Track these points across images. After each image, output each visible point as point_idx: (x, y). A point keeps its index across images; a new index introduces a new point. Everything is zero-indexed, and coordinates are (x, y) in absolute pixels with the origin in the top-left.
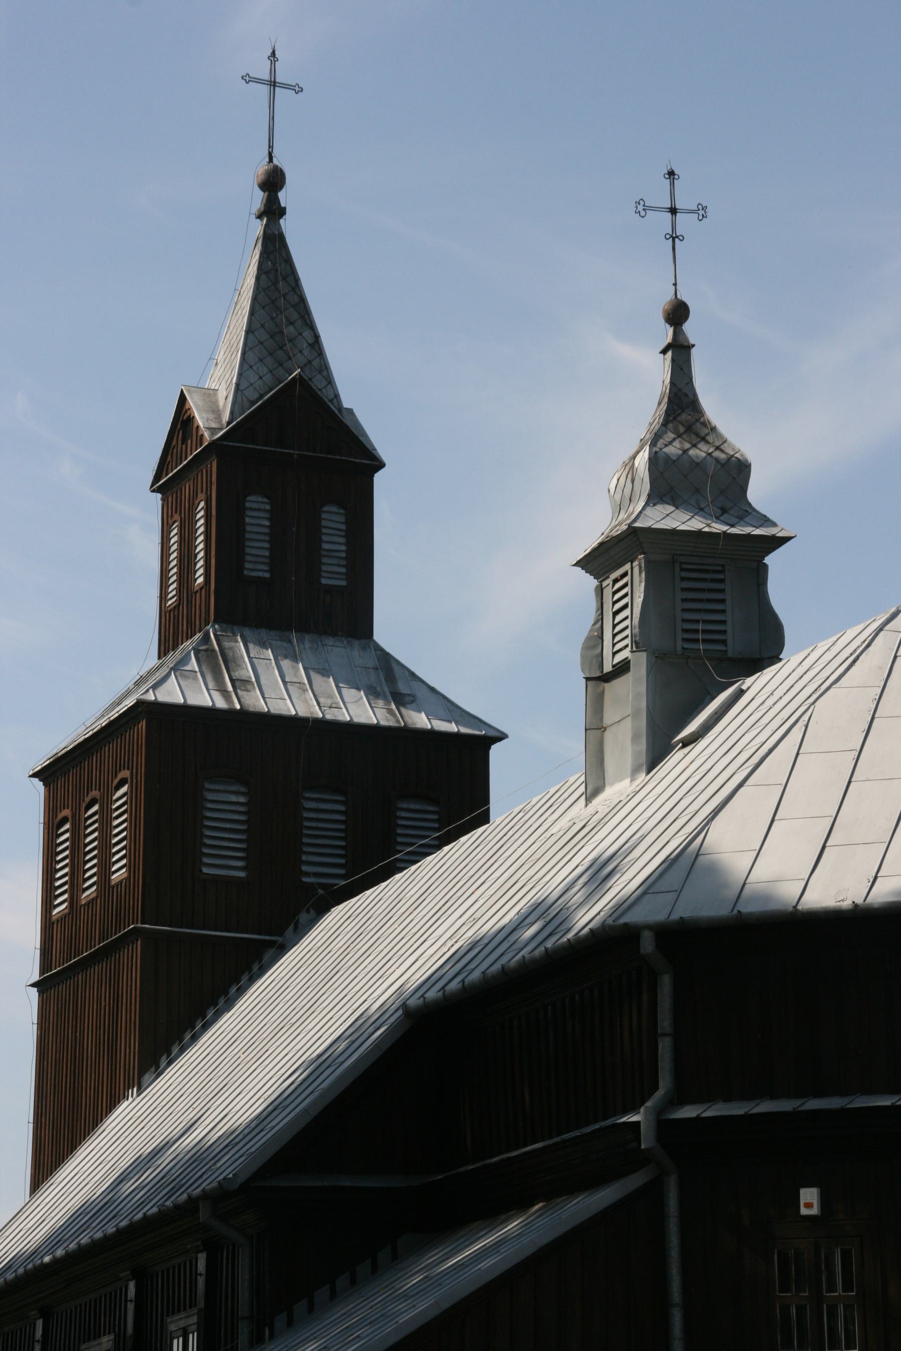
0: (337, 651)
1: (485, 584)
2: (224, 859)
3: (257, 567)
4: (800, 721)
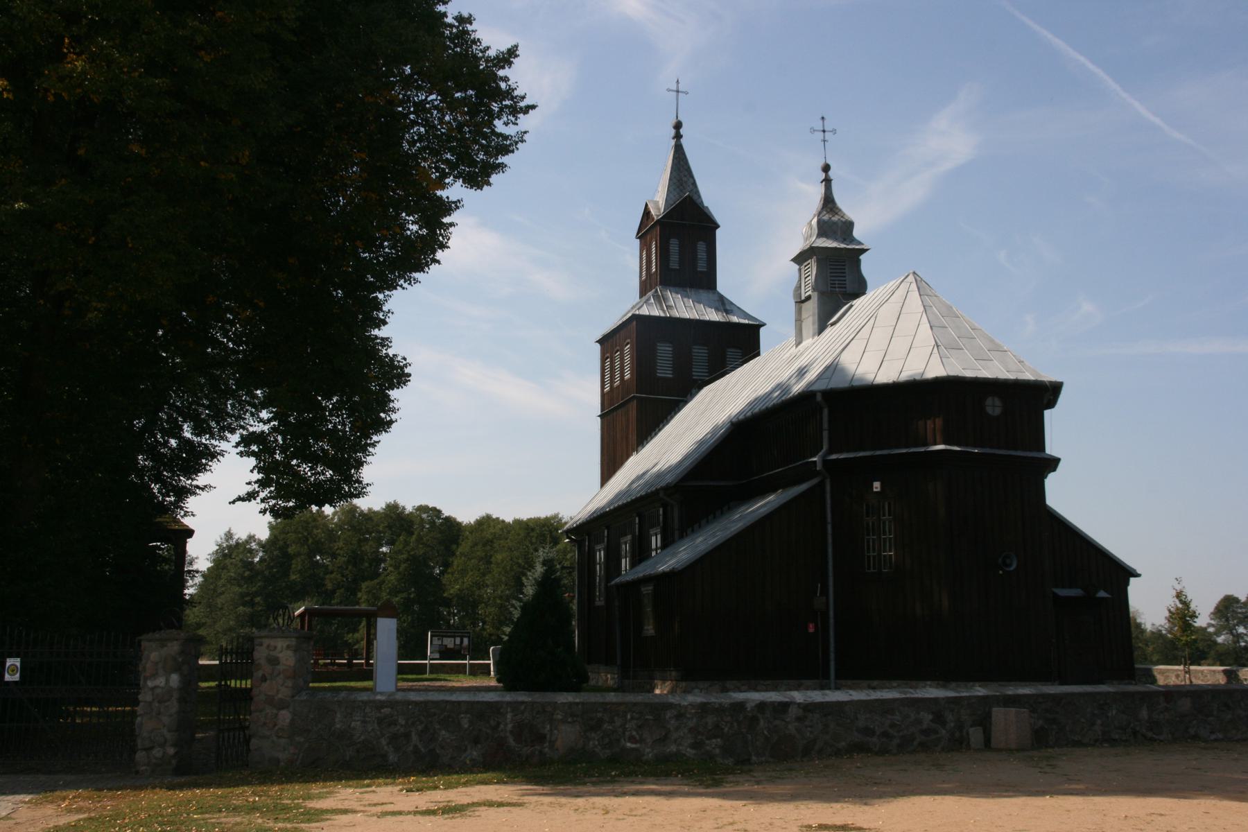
0: (704, 294)
1: (758, 269)
2: (664, 370)
3: (674, 265)
4: (874, 316)
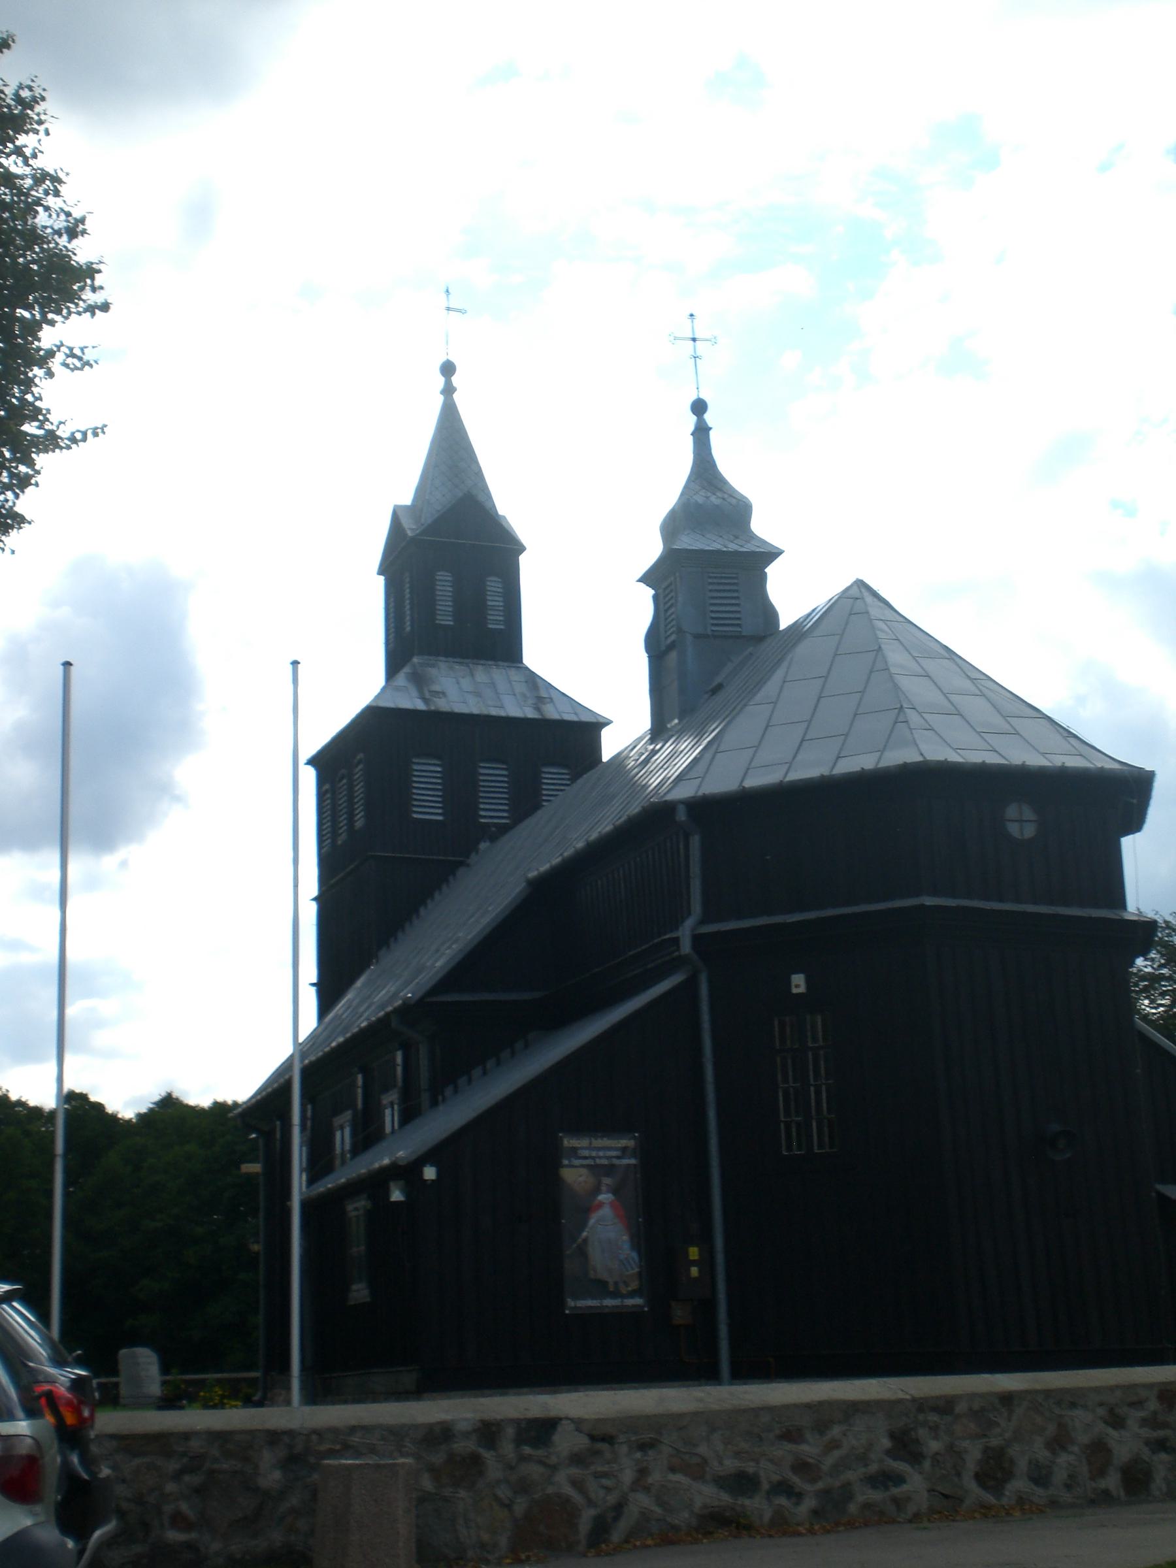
2: (427, 805)
